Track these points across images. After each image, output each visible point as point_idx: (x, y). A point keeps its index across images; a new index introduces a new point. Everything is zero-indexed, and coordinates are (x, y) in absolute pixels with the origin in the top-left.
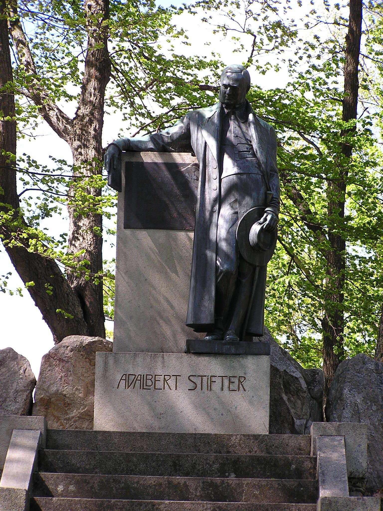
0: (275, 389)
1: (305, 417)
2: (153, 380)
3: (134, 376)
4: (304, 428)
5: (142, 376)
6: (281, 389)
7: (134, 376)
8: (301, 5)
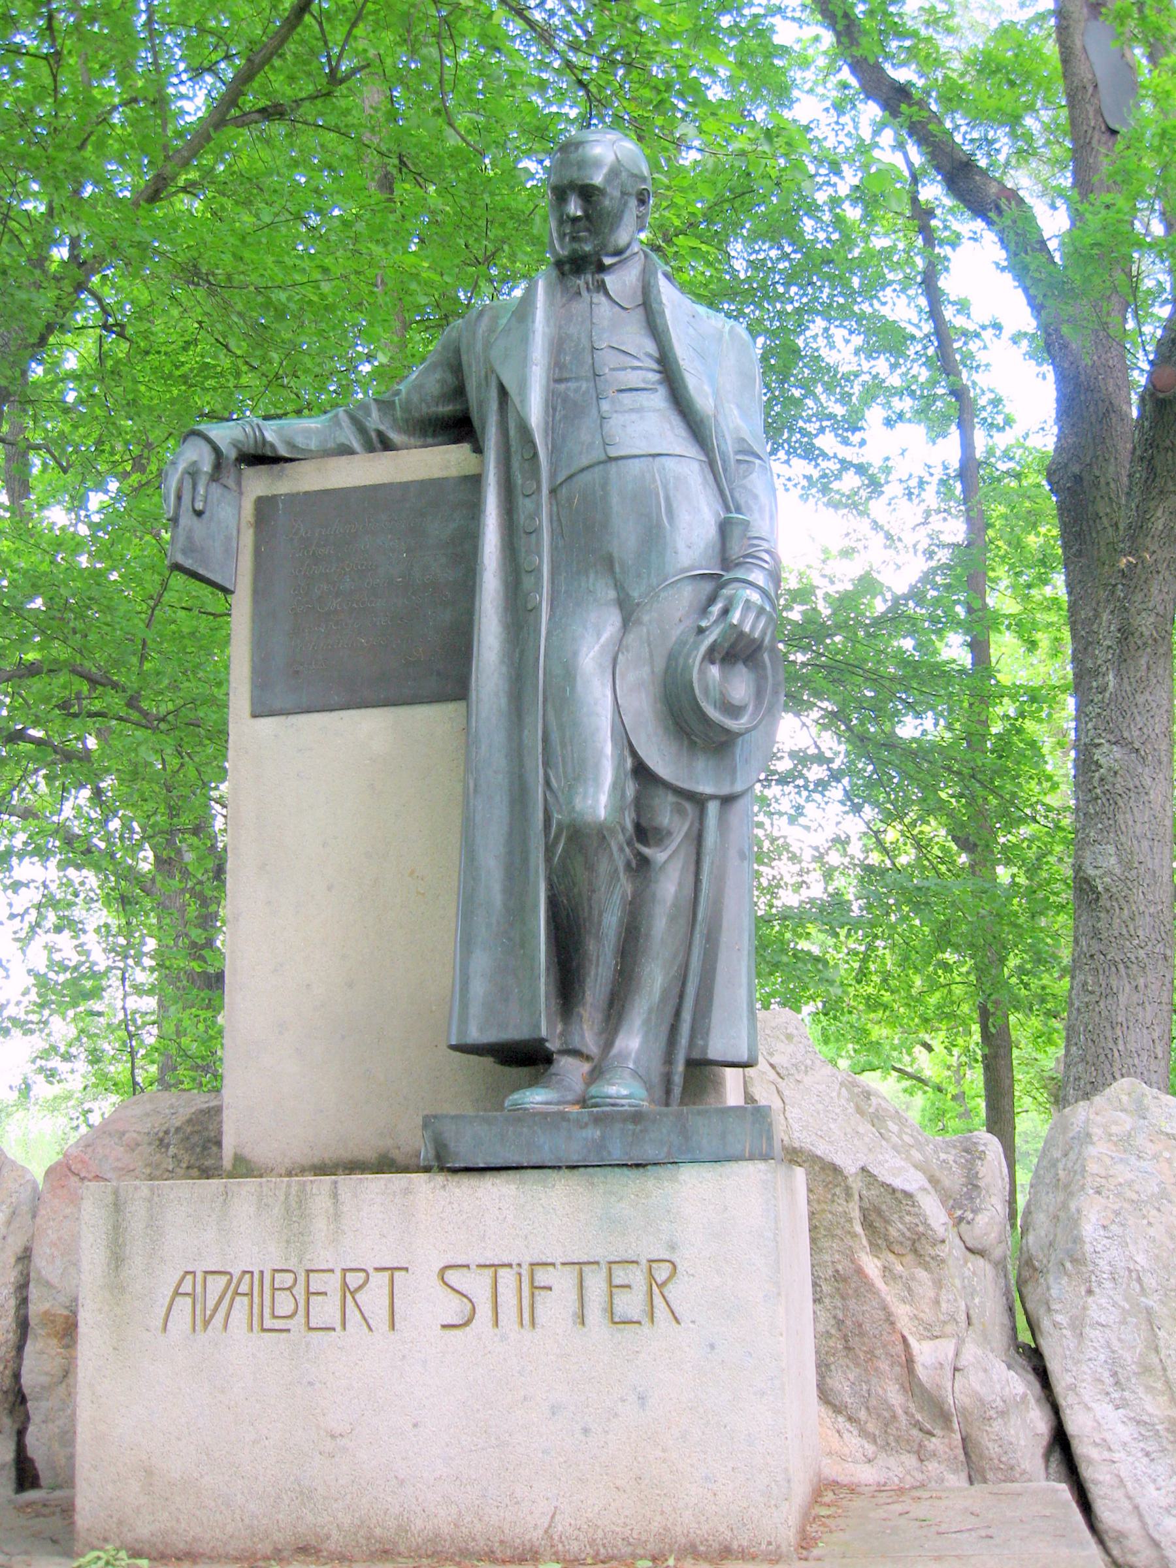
0: (833, 1236)
1: (949, 1329)
2: (300, 1290)
3: (225, 1278)
4: (950, 1375)
5: (256, 1276)
6: (855, 1235)
7: (225, 1278)
8: (892, 427)
